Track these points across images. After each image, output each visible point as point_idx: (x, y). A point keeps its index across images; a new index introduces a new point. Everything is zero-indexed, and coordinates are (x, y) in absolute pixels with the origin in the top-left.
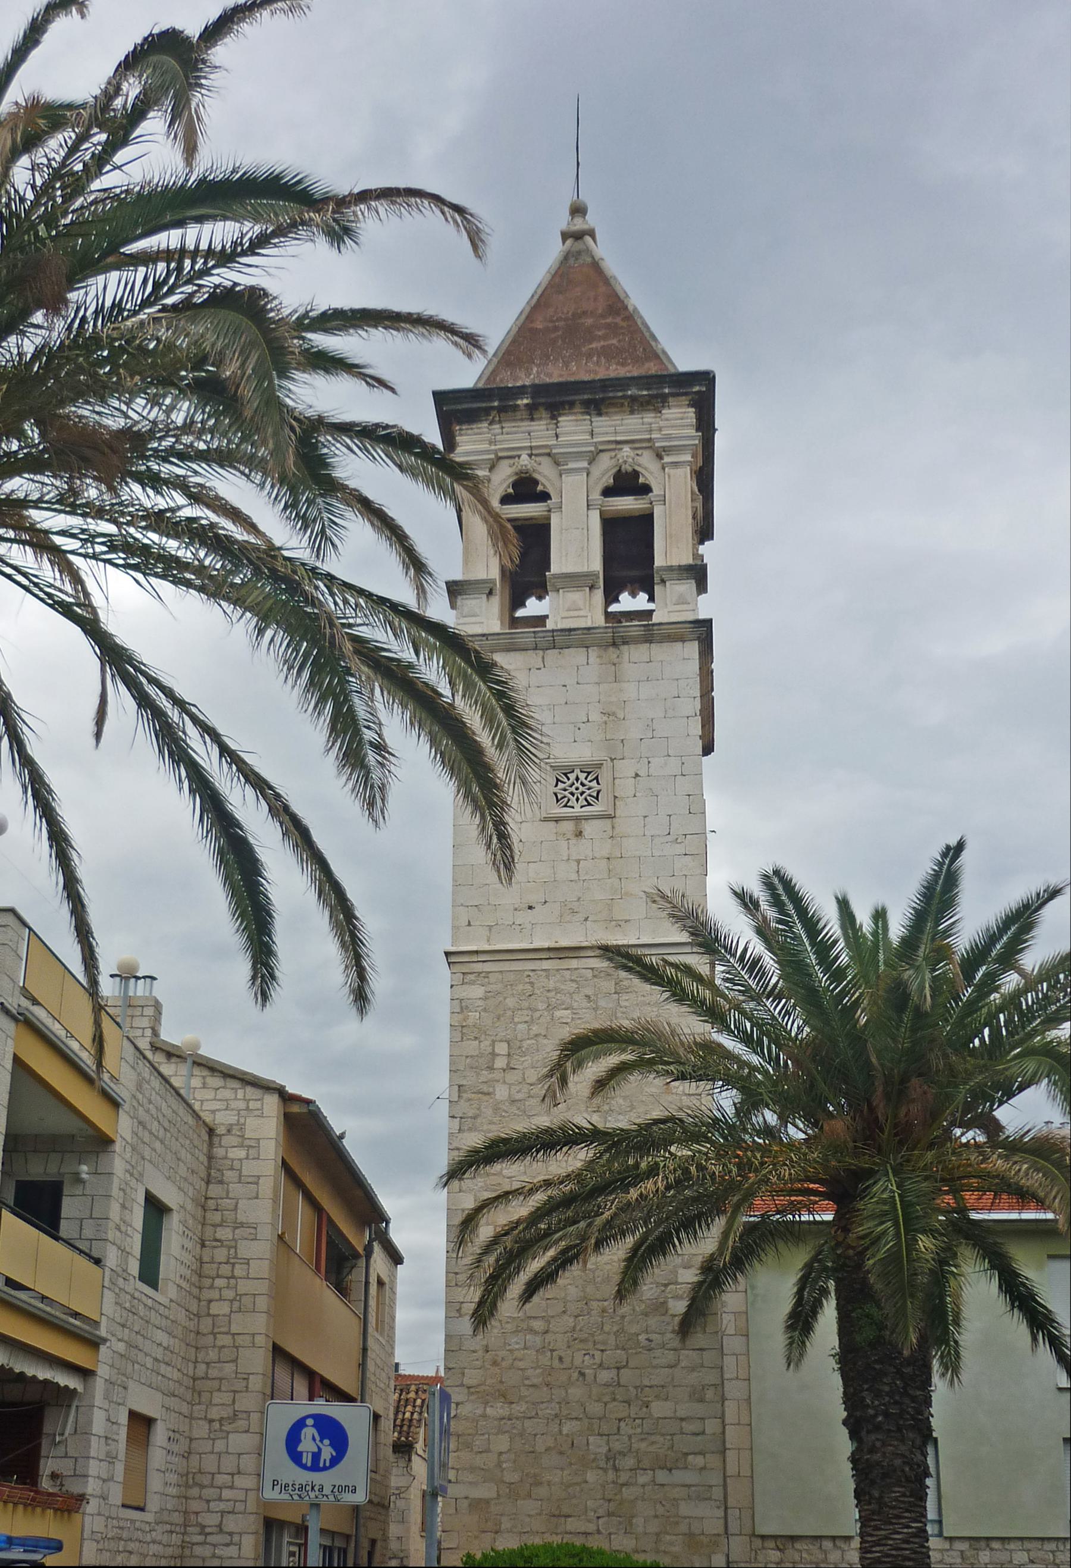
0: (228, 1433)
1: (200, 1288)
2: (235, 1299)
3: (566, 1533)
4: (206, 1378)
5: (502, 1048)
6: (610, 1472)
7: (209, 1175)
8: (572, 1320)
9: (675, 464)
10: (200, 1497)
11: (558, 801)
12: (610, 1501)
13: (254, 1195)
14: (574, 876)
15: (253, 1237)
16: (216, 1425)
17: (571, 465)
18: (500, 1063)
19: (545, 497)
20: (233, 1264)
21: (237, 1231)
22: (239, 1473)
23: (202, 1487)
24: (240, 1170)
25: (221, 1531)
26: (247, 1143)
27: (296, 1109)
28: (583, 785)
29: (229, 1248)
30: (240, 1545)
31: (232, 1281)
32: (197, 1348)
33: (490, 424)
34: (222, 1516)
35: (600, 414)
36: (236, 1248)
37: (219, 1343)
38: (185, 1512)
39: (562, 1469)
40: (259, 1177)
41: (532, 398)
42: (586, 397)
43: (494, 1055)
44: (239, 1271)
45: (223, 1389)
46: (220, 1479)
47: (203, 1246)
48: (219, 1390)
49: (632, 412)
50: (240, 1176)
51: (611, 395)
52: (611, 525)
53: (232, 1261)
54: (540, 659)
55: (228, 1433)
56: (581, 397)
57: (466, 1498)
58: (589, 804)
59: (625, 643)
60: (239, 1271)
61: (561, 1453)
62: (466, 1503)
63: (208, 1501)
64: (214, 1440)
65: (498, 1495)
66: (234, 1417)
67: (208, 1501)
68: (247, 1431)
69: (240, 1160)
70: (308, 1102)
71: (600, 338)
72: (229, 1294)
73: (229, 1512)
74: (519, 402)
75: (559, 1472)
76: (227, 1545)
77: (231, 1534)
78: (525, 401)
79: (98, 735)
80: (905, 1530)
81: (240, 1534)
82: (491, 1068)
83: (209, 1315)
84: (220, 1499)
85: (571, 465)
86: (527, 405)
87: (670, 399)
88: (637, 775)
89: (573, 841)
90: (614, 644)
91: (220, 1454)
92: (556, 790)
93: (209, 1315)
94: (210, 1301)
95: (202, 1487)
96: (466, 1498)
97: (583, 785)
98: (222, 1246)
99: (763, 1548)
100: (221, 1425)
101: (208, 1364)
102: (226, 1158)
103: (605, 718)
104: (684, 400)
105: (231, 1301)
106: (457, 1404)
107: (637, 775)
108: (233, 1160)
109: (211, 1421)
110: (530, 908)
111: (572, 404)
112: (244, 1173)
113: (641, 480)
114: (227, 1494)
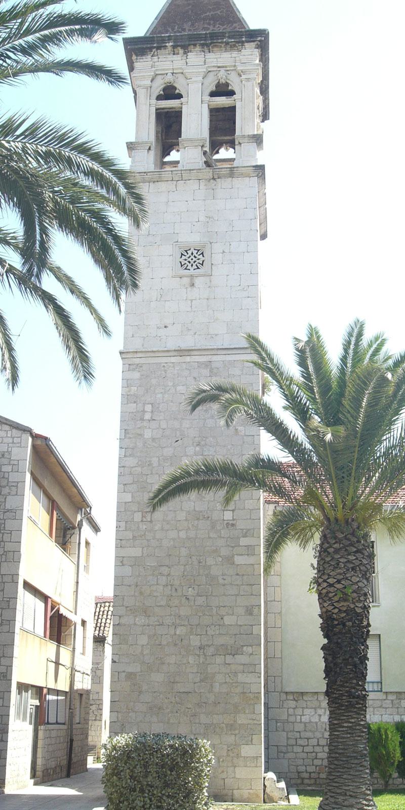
5: (148, 408)
14: (189, 309)
18: (147, 416)
19: (179, 96)
24: (8, 479)
26: (12, 462)
27: (39, 442)
28: (195, 257)
33: (152, 56)
41: (174, 42)
43: (144, 411)
52: (215, 112)
57: (124, 672)
58: (198, 268)
61: (175, 645)
62: (124, 674)
69: (9, 472)
70: (46, 439)
71: (210, 10)
82: (142, 419)
87: (246, 44)
88: (224, 252)
89: (189, 289)
90: (214, 179)
92: (181, 260)
96: (124, 672)
97: (195, 257)
103: (208, 220)
104: (253, 45)
107: (224, 252)
110: (165, 327)
113: (230, 88)
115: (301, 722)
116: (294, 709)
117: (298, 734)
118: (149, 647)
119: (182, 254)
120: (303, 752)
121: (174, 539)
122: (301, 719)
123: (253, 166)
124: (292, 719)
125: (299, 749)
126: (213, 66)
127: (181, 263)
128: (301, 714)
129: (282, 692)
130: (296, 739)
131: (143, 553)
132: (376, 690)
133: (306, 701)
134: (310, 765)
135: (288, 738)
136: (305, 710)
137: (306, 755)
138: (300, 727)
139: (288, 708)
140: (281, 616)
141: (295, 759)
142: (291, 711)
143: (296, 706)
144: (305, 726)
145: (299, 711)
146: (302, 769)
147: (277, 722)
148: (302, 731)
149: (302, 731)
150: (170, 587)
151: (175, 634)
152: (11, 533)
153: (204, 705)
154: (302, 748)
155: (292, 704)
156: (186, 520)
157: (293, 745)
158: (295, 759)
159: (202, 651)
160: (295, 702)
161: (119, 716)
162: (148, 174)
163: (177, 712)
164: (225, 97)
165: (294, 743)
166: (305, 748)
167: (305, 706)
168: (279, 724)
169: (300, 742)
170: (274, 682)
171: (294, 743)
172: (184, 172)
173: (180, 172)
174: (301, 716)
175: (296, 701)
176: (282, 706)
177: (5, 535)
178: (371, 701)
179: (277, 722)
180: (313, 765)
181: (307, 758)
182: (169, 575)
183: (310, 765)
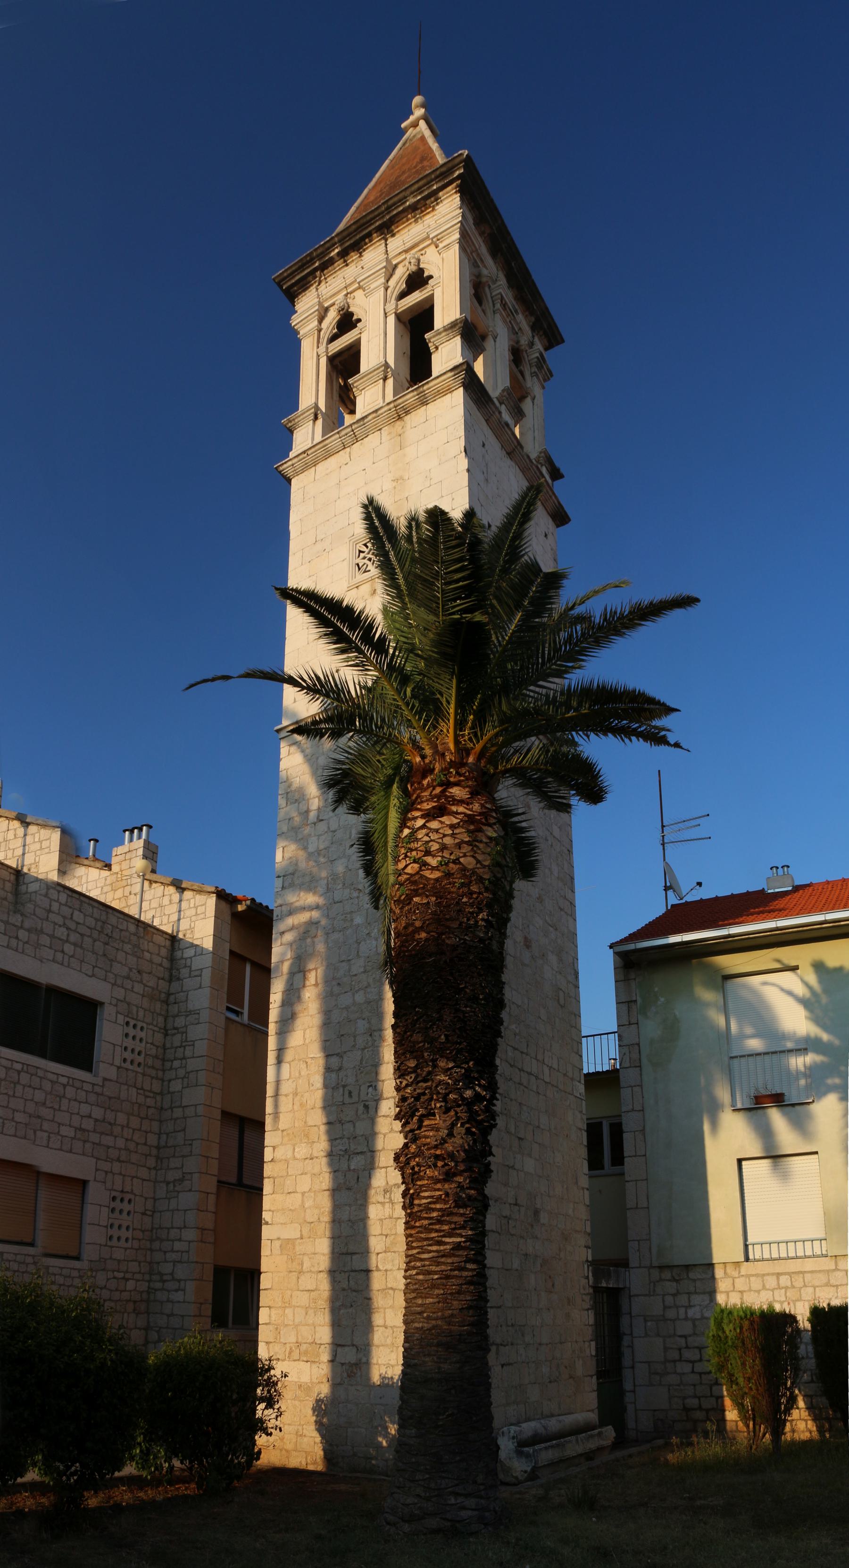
0: (178, 1192)
1: (164, 1071)
2: (185, 1077)
3: (352, 1271)
4: (166, 1147)
6: (387, 1205)
7: (171, 975)
8: (360, 1052)
9: (447, 246)
10: (160, 1250)
11: (359, 569)
12: (386, 1236)
13: (198, 986)
15: (197, 1021)
16: (171, 1186)
17: (372, 286)
20: (185, 1047)
21: (188, 1019)
22: (185, 1227)
23: (162, 1240)
24: (190, 967)
25: (173, 1279)
29: (183, 1033)
30: (184, 1290)
31: (184, 1061)
32: (161, 1121)
34: (174, 1265)
35: (393, 235)
36: (186, 1032)
37: (175, 1116)
38: (150, 1263)
39: (350, 1206)
40: (201, 969)
41: (341, 245)
42: (377, 224)
44: (188, 1053)
45: (177, 1154)
46: (173, 1233)
47: (166, 1035)
48: (174, 1156)
49: (416, 221)
50: (191, 971)
51: (395, 212)
53: (184, 1044)
54: (348, 456)
55: (178, 1192)
56: (373, 227)
57: (279, 1239)
59: (407, 413)
60: (188, 1053)
61: (349, 1189)
62: (277, 1244)
63: (165, 1252)
64: (169, 1199)
65: (301, 1235)
66: (182, 1180)
67: (165, 1252)
68: (190, 1190)
72: (181, 1073)
73: (178, 1262)
74: (332, 254)
75: (347, 1208)
76: (177, 1290)
77: (179, 1281)
78: (336, 251)
79: (187, 689)
80: (434, 1248)
81: (185, 1280)
83: (169, 1092)
84: (172, 1251)
85: (372, 286)
86: (338, 254)
90: (400, 418)
91: (173, 1211)
92: (358, 561)
93: (169, 1092)
94: (170, 1081)
95: (162, 1240)
96: (279, 1239)
98: (178, 1033)
99: (661, 1280)
100: (174, 1186)
101: (167, 1134)
102: (182, 958)
103: (394, 484)
105: (182, 1078)
106: (274, 1148)
108: (186, 959)
109: (168, 1183)
111: (369, 235)
112: (193, 968)
114: (177, 1246)
115: (686, 1319)
116: (674, 1295)
117: (683, 1341)
118: (312, 1194)
119: (360, 552)
120: (693, 1372)
121: (347, 1008)
122: (686, 1313)
123: (451, 370)
124: (671, 1314)
125: (687, 1368)
126: (400, 253)
127: (358, 565)
128: (687, 1304)
129: (651, 1267)
130: (680, 1349)
131: (305, 1039)
132: (819, 1253)
133: (694, 1281)
134: (706, 1397)
135: (666, 1349)
136: (693, 1297)
137: (698, 1377)
138: (685, 1328)
139: (664, 1295)
140: (644, 1135)
141: (679, 1385)
142: (669, 1300)
143: (678, 1290)
144: (695, 1326)
145: (683, 1300)
146: (693, 1402)
147: (646, 1321)
148: (690, 1336)
149: (690, 1336)
150: (341, 1089)
151: (349, 1170)
152: (193, 1045)
153: (391, 1292)
154: (691, 1365)
155: (671, 1287)
156: (365, 972)
157: (674, 1361)
158: (679, 1385)
159: (388, 1195)
160: (674, 1284)
161: (272, 1314)
162: (309, 452)
163: (352, 1306)
164: (417, 292)
165: (677, 1357)
166: (696, 1364)
167: (692, 1289)
168: (649, 1324)
169: (687, 1354)
170: (639, 1250)
171: (677, 1357)
172: (356, 426)
173: (349, 429)
174: (686, 1307)
175: (677, 1281)
176: (654, 1290)
177: (187, 1048)
178: (809, 1275)
179: (646, 1321)
180: (712, 1396)
181: (701, 1383)
182: (340, 1069)
183: (706, 1397)
